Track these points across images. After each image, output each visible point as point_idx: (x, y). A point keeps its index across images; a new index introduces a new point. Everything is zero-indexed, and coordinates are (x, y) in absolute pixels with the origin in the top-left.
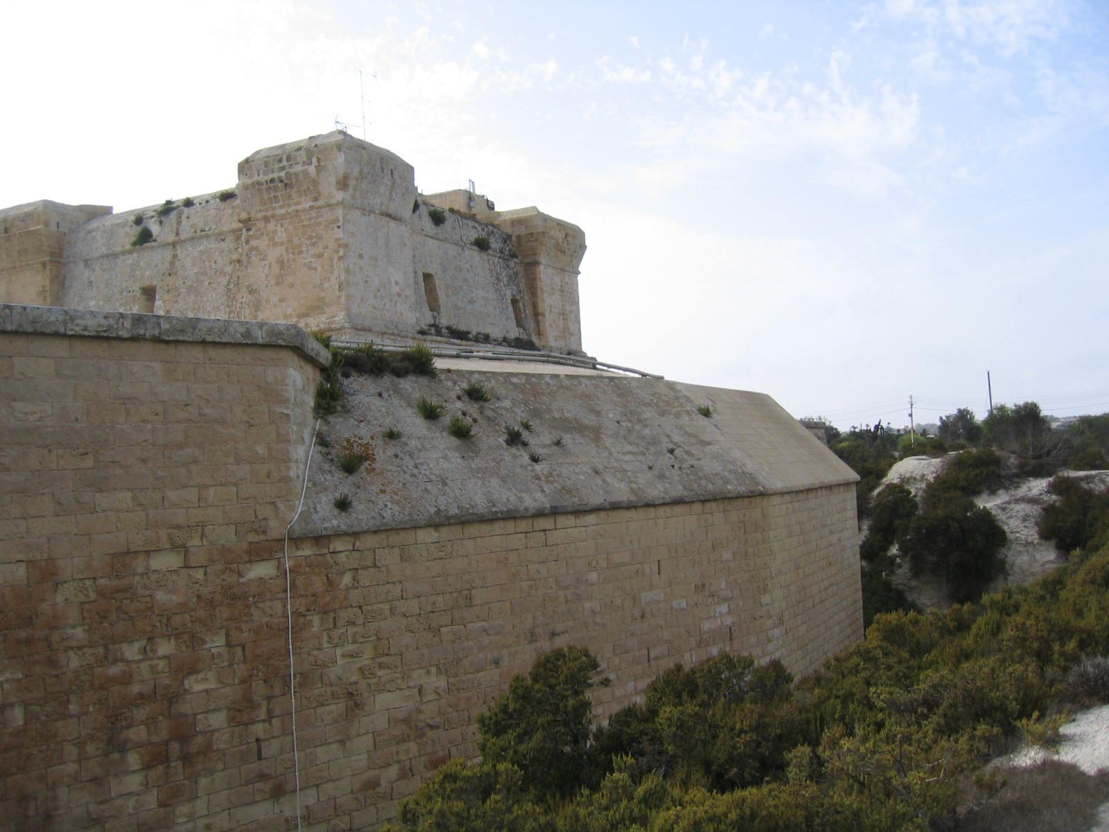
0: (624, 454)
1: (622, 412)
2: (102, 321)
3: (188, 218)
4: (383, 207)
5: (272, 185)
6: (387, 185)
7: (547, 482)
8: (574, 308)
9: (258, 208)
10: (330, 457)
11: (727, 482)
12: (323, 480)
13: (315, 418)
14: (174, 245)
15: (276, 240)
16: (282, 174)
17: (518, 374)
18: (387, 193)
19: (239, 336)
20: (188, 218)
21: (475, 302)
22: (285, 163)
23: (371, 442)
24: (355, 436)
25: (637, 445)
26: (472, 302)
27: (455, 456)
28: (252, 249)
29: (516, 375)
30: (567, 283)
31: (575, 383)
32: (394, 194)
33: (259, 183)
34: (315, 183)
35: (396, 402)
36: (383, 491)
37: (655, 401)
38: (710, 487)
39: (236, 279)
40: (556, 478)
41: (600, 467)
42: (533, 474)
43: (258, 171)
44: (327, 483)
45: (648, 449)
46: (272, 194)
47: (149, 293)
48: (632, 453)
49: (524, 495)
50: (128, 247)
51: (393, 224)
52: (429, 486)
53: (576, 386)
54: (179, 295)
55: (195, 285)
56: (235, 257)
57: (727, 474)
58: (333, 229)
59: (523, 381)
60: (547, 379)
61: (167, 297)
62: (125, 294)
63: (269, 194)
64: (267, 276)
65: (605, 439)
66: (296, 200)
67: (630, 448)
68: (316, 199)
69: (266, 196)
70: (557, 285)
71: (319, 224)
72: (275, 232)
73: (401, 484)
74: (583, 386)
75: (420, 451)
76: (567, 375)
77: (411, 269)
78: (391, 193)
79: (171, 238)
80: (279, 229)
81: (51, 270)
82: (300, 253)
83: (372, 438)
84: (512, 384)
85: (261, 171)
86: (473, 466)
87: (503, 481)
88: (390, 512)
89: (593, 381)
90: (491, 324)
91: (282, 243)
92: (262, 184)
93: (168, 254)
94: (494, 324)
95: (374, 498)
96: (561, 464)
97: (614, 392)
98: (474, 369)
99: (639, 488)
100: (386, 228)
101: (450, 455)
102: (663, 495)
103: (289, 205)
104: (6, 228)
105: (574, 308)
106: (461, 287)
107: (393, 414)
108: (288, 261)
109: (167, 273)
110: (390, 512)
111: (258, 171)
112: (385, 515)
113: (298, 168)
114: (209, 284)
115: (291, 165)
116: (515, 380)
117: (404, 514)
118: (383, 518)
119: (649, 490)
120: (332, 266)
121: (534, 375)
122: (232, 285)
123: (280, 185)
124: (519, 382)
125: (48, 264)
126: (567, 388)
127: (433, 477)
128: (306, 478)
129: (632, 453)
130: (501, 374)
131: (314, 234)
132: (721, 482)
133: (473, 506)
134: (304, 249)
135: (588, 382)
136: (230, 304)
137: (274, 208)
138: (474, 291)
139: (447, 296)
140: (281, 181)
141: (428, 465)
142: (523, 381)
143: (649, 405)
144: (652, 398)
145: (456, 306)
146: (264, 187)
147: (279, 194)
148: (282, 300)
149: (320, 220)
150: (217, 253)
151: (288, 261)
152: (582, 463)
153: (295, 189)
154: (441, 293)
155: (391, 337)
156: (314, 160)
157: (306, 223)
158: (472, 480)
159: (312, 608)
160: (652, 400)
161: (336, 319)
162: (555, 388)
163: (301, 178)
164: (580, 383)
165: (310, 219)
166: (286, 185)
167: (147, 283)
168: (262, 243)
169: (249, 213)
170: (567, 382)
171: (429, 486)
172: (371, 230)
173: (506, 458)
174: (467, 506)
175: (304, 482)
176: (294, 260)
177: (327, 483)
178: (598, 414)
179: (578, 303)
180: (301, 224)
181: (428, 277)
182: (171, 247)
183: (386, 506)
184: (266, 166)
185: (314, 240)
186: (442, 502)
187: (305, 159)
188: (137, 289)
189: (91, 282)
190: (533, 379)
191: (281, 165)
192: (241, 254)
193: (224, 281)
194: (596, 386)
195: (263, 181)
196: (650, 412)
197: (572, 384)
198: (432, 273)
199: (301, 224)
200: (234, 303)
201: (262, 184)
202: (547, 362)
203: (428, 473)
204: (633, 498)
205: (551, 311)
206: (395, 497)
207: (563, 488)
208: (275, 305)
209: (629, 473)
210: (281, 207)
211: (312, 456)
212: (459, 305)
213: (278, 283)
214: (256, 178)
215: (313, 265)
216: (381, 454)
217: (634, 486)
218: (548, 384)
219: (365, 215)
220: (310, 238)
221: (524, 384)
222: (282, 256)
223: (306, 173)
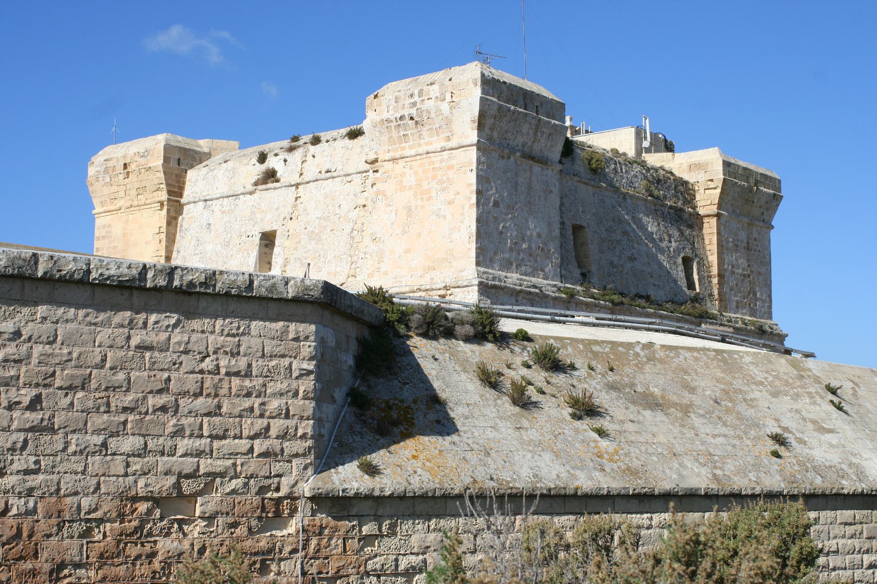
0: (714, 436)
1: (724, 390)
2: (126, 271)
3: (314, 157)
4: (526, 149)
5: (402, 122)
6: (531, 124)
7: (610, 460)
8: (763, 270)
9: (386, 148)
10: (364, 418)
11: (843, 477)
12: (351, 441)
13: (355, 376)
14: (297, 185)
15: (404, 184)
16: (413, 111)
17: (603, 342)
18: (531, 133)
19: (263, 290)
20: (314, 157)
21: (635, 259)
22: (416, 98)
23: (412, 405)
24: (396, 399)
25: (735, 428)
26: (632, 259)
27: (506, 429)
28: (378, 193)
29: (596, 342)
30: (755, 239)
31: (672, 355)
32: (539, 134)
33: (388, 121)
34: (448, 122)
35: (451, 365)
36: (414, 457)
37: (770, 379)
38: (818, 481)
39: (360, 225)
40: (622, 457)
41: (678, 449)
42: (596, 451)
43: (388, 107)
44: (355, 445)
45: (746, 433)
46: (402, 133)
47: (268, 240)
48: (725, 436)
49: (578, 473)
50: (250, 188)
51: (537, 168)
52: (469, 455)
53: (672, 358)
54: (299, 242)
55: (317, 231)
56: (362, 202)
57: (844, 466)
58: (465, 173)
59: (607, 350)
60: (638, 349)
61: (287, 243)
62: (243, 238)
63: (399, 132)
64: (392, 224)
65: (694, 418)
66: (427, 140)
67: (724, 430)
68: (448, 139)
69: (395, 134)
70: (742, 241)
71: (450, 167)
72: (403, 175)
73: (437, 452)
74: (681, 358)
75: (466, 418)
76: (664, 346)
77: (557, 219)
78: (535, 134)
79: (296, 179)
80: (407, 170)
81: (168, 210)
82: (429, 199)
83: (415, 402)
84: (592, 352)
85: (391, 107)
86: (525, 438)
87: (557, 456)
88: (418, 478)
89: (695, 354)
90: (654, 285)
91: (410, 188)
92: (391, 121)
93: (292, 192)
94: (659, 286)
95: (403, 463)
96: (632, 442)
97: (719, 367)
98: (550, 334)
99: (724, 475)
100: (528, 173)
101: (500, 424)
102: (753, 485)
103: (420, 145)
104: (125, 164)
105: (763, 270)
106: (618, 242)
107: (444, 379)
108: (416, 207)
109: (288, 217)
110: (418, 478)
111: (388, 107)
112: (412, 482)
113: (429, 104)
114: (332, 230)
115: (423, 100)
116: (596, 348)
117: (433, 482)
118: (410, 484)
119: (736, 479)
120: (462, 214)
121: (622, 344)
122: (355, 232)
123: (411, 122)
124: (601, 350)
125: (165, 203)
126: (662, 361)
127: (475, 446)
128: (333, 437)
129: (725, 436)
130: (582, 341)
131: (445, 178)
132: (835, 476)
133: (515, 480)
134: (434, 194)
135: (688, 355)
136: (352, 253)
137: (403, 149)
138: (636, 246)
139: (602, 251)
140: (412, 118)
141: (473, 433)
142: (607, 350)
143: (762, 383)
144: (766, 375)
145: (612, 264)
146: (394, 124)
147: (409, 132)
148: (407, 251)
149: (451, 163)
150: (342, 197)
151: (416, 207)
152: (660, 443)
153: (427, 127)
154: (593, 248)
155: (528, 297)
156: (448, 95)
157: (437, 165)
158: (520, 453)
159: (325, 571)
160: (766, 378)
161: (464, 274)
162: (645, 359)
163: (433, 115)
164: (678, 355)
165: (442, 161)
166: (417, 123)
167: (268, 228)
168: (388, 187)
169: (376, 153)
170: (662, 354)
171: (469, 455)
172: (509, 175)
173: (566, 431)
174: (509, 479)
175: (329, 442)
176: (423, 207)
177: (355, 445)
178: (692, 390)
179: (769, 263)
180: (431, 167)
181: (577, 229)
182: (294, 188)
183: (415, 472)
184: (396, 102)
185: (445, 185)
186: (481, 474)
187: (438, 94)
188: (257, 233)
189: (209, 224)
190: (620, 349)
191: (412, 100)
192: (366, 199)
193: (348, 228)
194: (696, 359)
195: (392, 118)
196: (761, 391)
197: (668, 356)
198: (584, 224)
199: (431, 167)
200: (357, 252)
201: (391, 121)
202: (614, 326)
203: (470, 441)
204: (714, 486)
205: (733, 273)
206: (428, 464)
207: (629, 469)
208: (400, 257)
209: (716, 458)
210: (411, 147)
211: (344, 416)
212: (616, 263)
213: (404, 232)
214: (385, 115)
215: (442, 213)
216: (421, 418)
217: (718, 472)
218: (637, 355)
219: (503, 157)
220: (441, 182)
221: (607, 354)
222: (409, 201)
223: (439, 112)
